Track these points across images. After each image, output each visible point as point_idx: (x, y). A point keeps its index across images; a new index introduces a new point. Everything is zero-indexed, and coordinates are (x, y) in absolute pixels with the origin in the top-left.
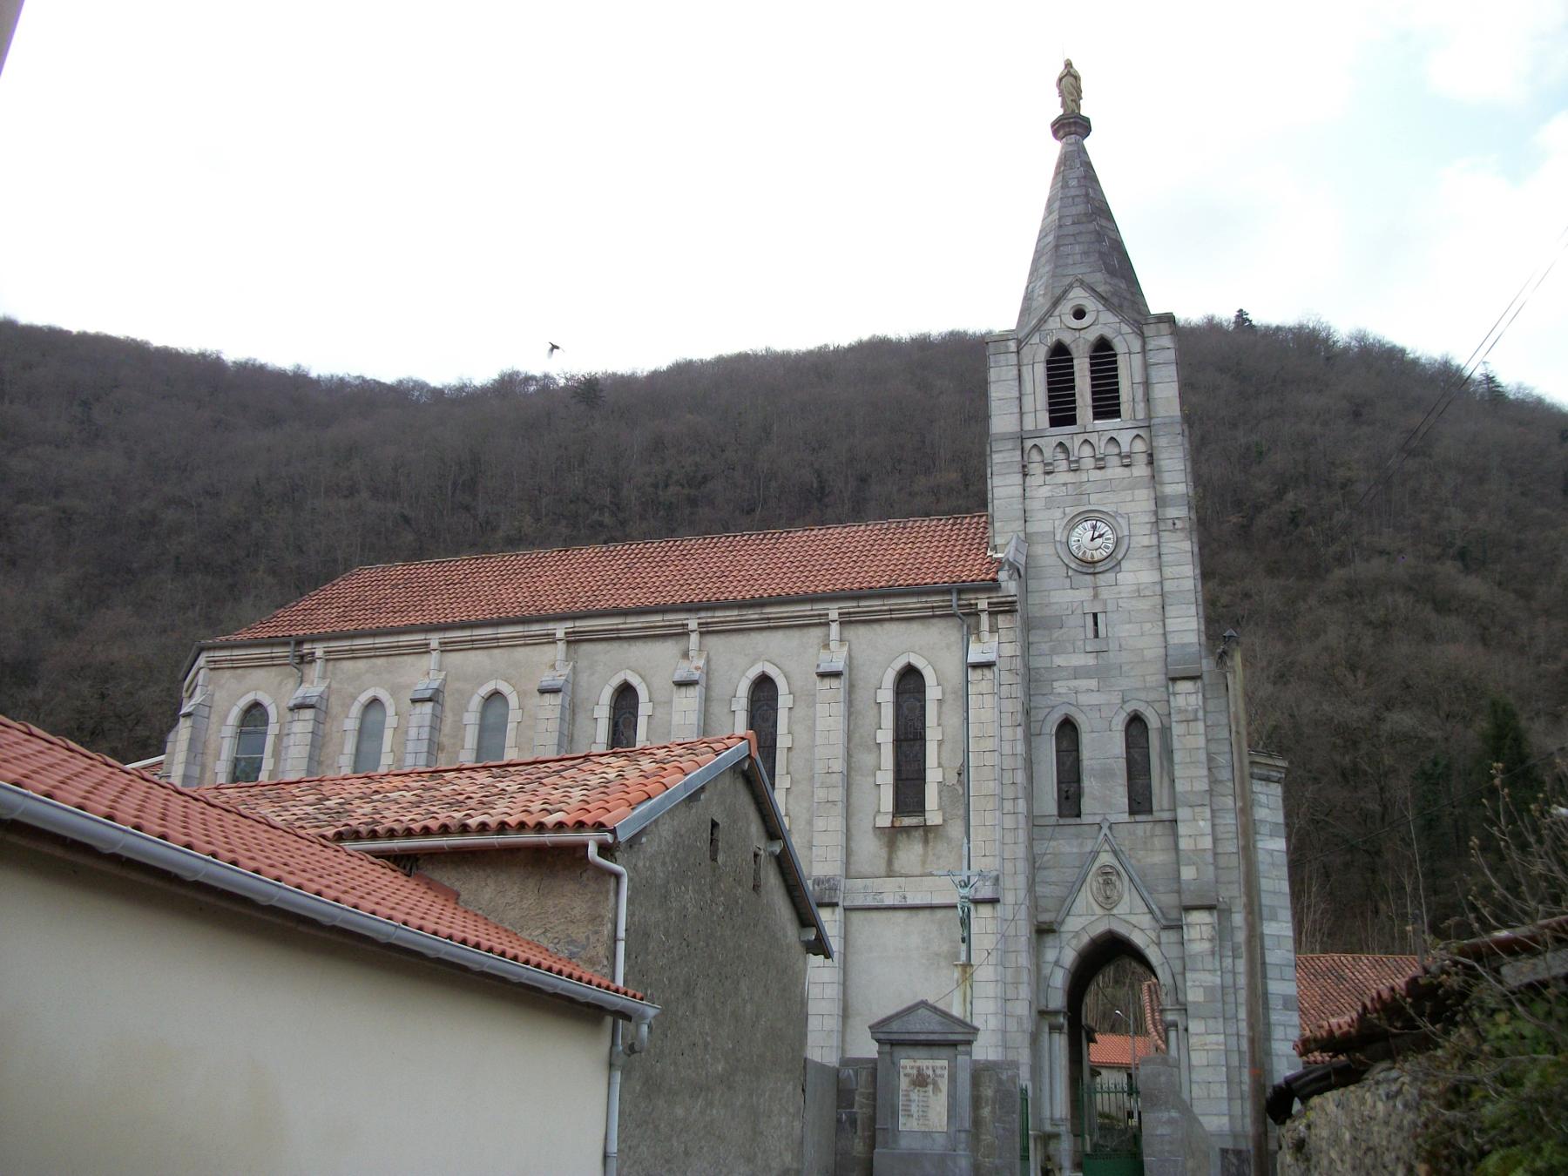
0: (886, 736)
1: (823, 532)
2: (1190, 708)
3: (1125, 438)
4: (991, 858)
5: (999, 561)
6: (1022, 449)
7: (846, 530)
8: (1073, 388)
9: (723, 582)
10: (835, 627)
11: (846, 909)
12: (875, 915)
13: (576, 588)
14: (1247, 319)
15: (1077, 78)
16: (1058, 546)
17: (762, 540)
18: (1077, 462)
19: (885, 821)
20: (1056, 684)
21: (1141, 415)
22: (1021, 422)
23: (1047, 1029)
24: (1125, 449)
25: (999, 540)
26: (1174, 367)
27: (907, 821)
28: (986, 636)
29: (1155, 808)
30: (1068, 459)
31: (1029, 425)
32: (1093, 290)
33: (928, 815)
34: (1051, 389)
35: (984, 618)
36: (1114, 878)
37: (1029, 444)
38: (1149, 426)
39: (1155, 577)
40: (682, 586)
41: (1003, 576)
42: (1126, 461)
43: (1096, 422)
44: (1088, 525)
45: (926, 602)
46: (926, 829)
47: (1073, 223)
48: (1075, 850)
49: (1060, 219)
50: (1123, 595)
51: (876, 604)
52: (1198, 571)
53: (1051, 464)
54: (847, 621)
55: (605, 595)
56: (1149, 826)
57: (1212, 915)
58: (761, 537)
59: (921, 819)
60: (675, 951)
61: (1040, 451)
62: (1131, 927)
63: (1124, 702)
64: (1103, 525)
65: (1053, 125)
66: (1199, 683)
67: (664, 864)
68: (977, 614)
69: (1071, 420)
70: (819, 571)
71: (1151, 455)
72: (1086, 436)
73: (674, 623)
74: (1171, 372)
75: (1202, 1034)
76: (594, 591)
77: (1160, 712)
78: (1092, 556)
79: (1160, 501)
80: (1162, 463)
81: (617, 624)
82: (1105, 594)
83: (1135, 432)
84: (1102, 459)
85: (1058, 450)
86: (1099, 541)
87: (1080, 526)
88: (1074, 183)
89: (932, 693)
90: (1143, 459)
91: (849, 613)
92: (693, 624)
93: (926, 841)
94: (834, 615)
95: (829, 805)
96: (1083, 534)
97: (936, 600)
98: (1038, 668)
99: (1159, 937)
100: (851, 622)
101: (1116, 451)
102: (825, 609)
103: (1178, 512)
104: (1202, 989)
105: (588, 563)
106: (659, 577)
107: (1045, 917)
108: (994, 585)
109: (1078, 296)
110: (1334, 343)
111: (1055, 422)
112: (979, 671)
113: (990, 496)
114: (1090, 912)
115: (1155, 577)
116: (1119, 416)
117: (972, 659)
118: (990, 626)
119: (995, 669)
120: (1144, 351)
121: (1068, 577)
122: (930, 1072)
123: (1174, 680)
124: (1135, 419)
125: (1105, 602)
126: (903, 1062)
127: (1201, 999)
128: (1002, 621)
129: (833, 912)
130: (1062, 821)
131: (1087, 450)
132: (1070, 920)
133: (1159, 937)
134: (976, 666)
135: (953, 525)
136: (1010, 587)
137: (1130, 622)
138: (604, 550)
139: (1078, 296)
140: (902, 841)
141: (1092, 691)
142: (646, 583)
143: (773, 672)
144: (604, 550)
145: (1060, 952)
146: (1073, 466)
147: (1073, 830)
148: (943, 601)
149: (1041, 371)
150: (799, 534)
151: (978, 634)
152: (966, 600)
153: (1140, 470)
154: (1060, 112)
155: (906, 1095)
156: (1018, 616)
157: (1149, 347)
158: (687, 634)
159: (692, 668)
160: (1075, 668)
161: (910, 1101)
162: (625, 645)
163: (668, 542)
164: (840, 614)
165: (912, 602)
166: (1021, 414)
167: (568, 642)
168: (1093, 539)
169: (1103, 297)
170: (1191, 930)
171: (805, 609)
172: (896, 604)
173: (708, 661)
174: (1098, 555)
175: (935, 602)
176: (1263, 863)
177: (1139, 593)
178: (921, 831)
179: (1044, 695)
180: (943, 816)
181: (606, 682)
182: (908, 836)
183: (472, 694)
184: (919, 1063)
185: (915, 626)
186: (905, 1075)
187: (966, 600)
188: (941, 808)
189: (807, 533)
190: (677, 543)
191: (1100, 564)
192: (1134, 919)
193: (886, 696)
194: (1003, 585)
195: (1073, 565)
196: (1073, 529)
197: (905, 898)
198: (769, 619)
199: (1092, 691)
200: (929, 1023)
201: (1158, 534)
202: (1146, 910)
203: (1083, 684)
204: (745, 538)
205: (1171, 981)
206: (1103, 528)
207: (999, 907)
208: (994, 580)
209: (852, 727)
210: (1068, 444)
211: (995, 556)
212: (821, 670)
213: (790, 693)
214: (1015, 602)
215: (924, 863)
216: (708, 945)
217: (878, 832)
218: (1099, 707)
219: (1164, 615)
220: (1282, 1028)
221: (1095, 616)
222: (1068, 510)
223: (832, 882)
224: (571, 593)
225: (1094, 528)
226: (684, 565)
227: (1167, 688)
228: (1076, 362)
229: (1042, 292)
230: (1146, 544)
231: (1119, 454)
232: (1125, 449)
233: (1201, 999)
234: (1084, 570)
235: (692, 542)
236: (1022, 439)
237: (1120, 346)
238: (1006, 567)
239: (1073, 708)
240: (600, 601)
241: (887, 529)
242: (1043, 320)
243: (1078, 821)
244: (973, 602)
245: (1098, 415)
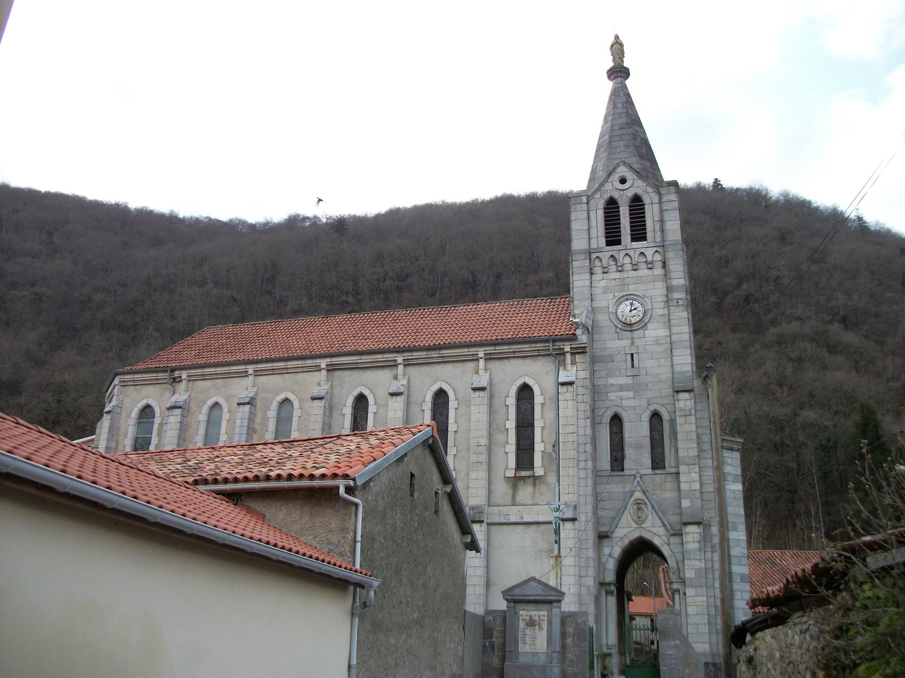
0: (511, 424)
1: (475, 307)
2: (687, 408)
3: (649, 253)
4: (572, 495)
5: (577, 323)
6: (590, 259)
7: (488, 305)
8: (619, 224)
9: (417, 336)
10: (482, 362)
11: (488, 524)
12: (505, 528)
13: (333, 339)
15: (621, 45)
16: (611, 315)
17: (440, 311)
18: (621, 266)
19: (511, 473)
20: (609, 395)
21: (658, 239)
22: (590, 243)
23: (604, 593)
24: (649, 259)
25: (576, 312)
26: (677, 212)
27: (524, 473)
28: (569, 366)
29: (666, 466)
30: (616, 265)
31: (594, 245)
32: (631, 167)
33: (535, 470)
34: (607, 224)
35: (568, 356)
36: (643, 506)
37: (594, 256)
38: (663, 246)
39: (667, 333)
40: (394, 338)
41: (579, 332)
42: (650, 266)
43: (633, 243)
44: (628, 303)
45: (535, 347)
46: (535, 478)
47: (620, 129)
48: (620, 490)
49: (612, 126)
50: (648, 343)
51: (505, 348)
52: (691, 329)
53: (606, 267)
54: (489, 358)
55: (349, 343)
56: (663, 476)
57: (699, 528)
58: (439, 309)
59: (532, 472)
60: (389, 548)
61: (601, 260)
62: (653, 534)
63: (649, 405)
64: (637, 303)
65: (608, 72)
66: (692, 394)
67: (383, 498)
68: (564, 354)
69: (618, 242)
70: (473, 329)
71: (664, 262)
72: (627, 251)
73: (389, 359)
74: (676, 215)
75: (694, 596)
76: (343, 341)
77: (670, 411)
78: (630, 320)
79: (669, 289)
80: (671, 267)
81: (356, 360)
82: (638, 342)
83: (655, 249)
84: (636, 265)
85: (611, 259)
86: (634, 312)
87: (623, 304)
88: (620, 105)
89: (538, 399)
90: (660, 264)
91: (490, 354)
92: (400, 360)
93: (534, 485)
94: (481, 354)
95: (479, 464)
96: (625, 308)
97: (540, 346)
98: (599, 385)
99: (669, 540)
100: (491, 359)
101: (644, 260)
102: (476, 351)
103: (680, 295)
104: (694, 570)
105: (339, 324)
106: (380, 333)
107: (603, 529)
108: (574, 337)
109: (622, 171)
110: (770, 197)
111: (609, 243)
112: (565, 387)
113: (571, 286)
114: (629, 526)
115: (667, 333)
116: (646, 240)
117: (561, 380)
119: (575, 385)
120: (660, 202)
121: (616, 332)
122: (537, 618)
123: (678, 392)
124: (655, 242)
126: (521, 612)
127: (693, 576)
128: (578, 358)
129: (481, 526)
130: (613, 474)
131: (627, 260)
133: (669, 540)
134: (563, 384)
135: (550, 303)
136: (583, 338)
137: (652, 359)
138: (348, 317)
139: (622, 171)
140: (521, 485)
141: (631, 398)
142: (373, 336)
143: (446, 387)
144: (348, 317)
145: (612, 549)
146: (620, 269)
147: (619, 478)
148: (544, 347)
149: (601, 214)
150: (461, 308)
151: (564, 366)
152: (557, 346)
153: (658, 271)
154: (612, 64)
155: (523, 632)
156: (587, 355)
157: (663, 200)
158: (396, 366)
159: (399, 385)
160: (621, 385)
161: (525, 635)
162: (361, 372)
163: (386, 312)
164: (485, 354)
165: (526, 347)
166: (590, 238)
167: (328, 370)
168: (631, 311)
169: (636, 171)
170: (687, 536)
171: (465, 351)
172: (517, 348)
173: (409, 381)
175: (540, 347)
176: (729, 497)
177: (657, 342)
178: (532, 479)
179: (602, 401)
180: (544, 470)
181: (350, 393)
182: (524, 482)
183: (273, 400)
184: (530, 613)
185: (528, 361)
186: (522, 620)
187: (557, 346)
188: (543, 466)
189: (466, 307)
190: (391, 313)
191: (635, 325)
192: (654, 530)
193: (512, 401)
194: (579, 337)
195: (619, 326)
196: (619, 305)
197: (522, 518)
198: (444, 357)
199: (631, 398)
200: (536, 590)
201: (668, 308)
202: (661, 525)
203: (625, 394)
204: (430, 310)
205: (676, 566)
206: (636, 305)
207: (576, 523)
208: (574, 334)
209: (491, 419)
210: (616, 256)
211: (574, 320)
212: (474, 386)
213: (456, 400)
214: (586, 347)
215: (533, 497)
216: (408, 545)
217: (507, 480)
218: (634, 408)
219: (672, 354)
220: (740, 593)
221: (632, 355)
222: (616, 294)
224: (330, 342)
225: (632, 304)
226: (395, 326)
227: (674, 397)
228: (621, 209)
230: (662, 313)
231: (646, 262)
232: (649, 259)
233: (693, 576)
234: (626, 329)
235: (400, 313)
236: (590, 253)
237: (646, 200)
238: (581, 327)
239: (619, 408)
240: (346, 346)
241: (512, 305)
242: (602, 185)
243: (622, 473)
244: (561, 347)
245: (634, 239)
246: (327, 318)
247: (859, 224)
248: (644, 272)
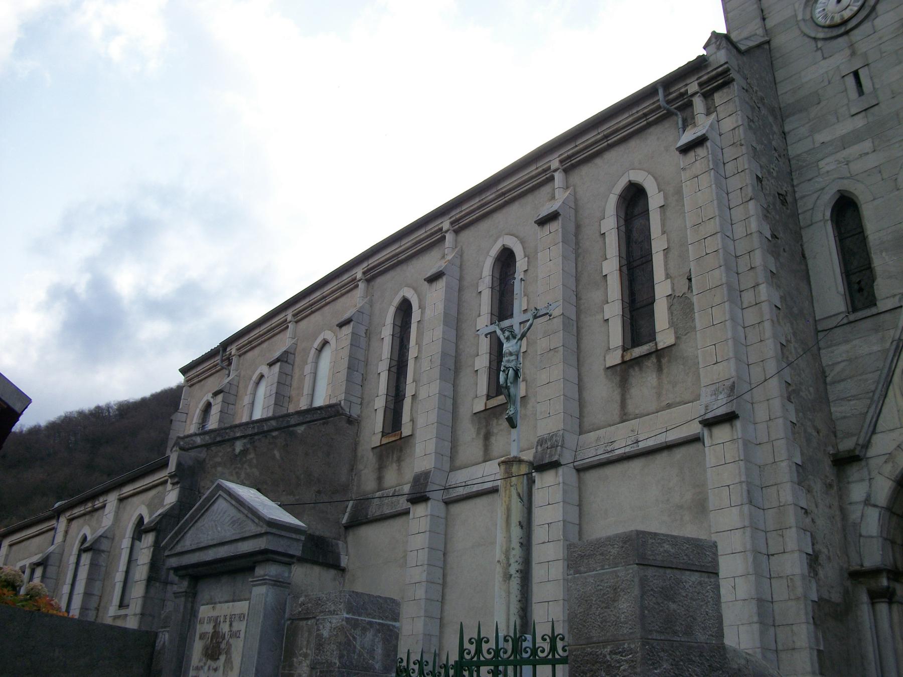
0: (611, 266)
4: (725, 363)
11: (579, 470)
12: (609, 471)
16: (802, 24)
19: (615, 358)
23: (865, 598)
27: (638, 352)
33: (659, 338)
46: (659, 354)
48: (875, 348)
59: (652, 344)
82: (862, 47)
93: (660, 369)
95: (552, 352)
98: (799, 155)
107: (846, 445)
121: (818, 49)
125: (865, 55)
129: (557, 473)
132: (876, 439)
141: (867, 154)
145: (870, 487)
147: (868, 324)
152: (675, 92)
156: (735, 87)
160: (842, 138)
162: (404, 267)
174: (847, 14)
178: (653, 359)
179: (809, 180)
180: (676, 333)
181: (390, 304)
182: (641, 369)
183: (311, 348)
185: (633, 143)
187: (675, 92)
188: (672, 324)
199: (867, 154)
203: (854, 150)
207: (738, 424)
209: (579, 269)
215: (659, 395)
217: (609, 372)
218: (879, 169)
223: (554, 438)
239: (845, 181)
243: (874, 310)
244: (683, 90)
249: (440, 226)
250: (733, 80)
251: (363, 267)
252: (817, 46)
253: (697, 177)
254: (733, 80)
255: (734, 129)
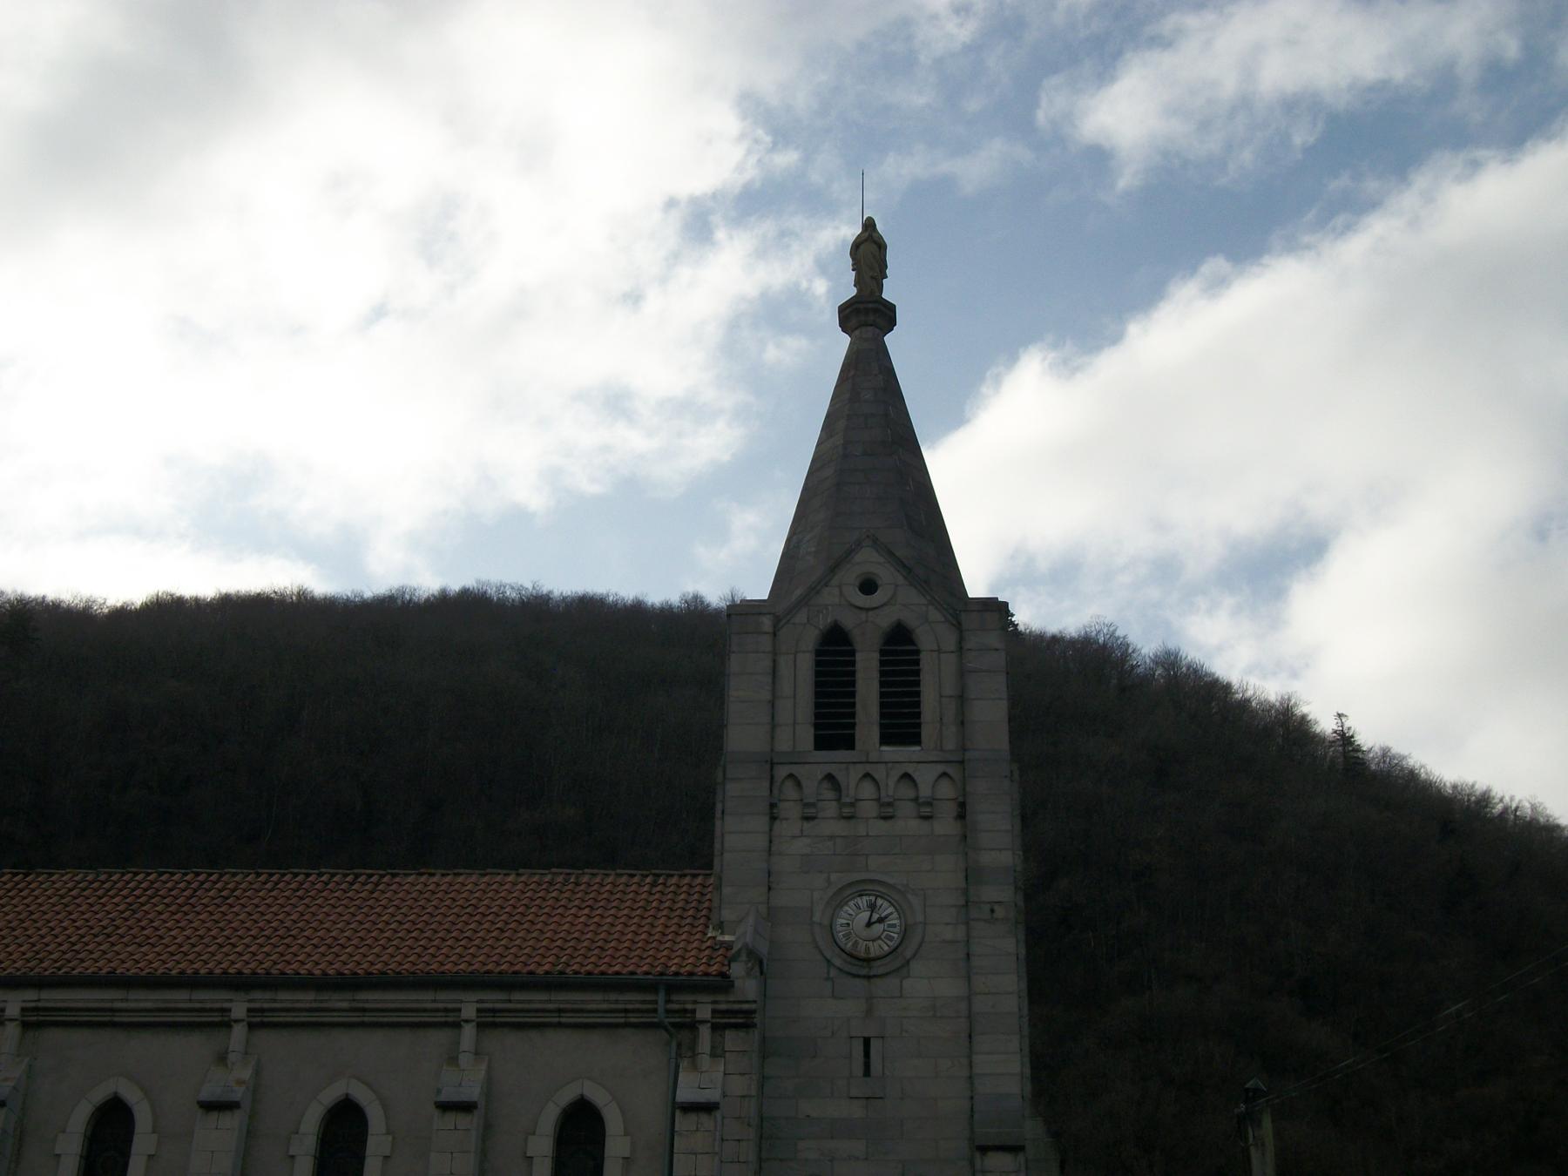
1: (448, 879)
3: (926, 777)
5: (728, 946)
6: (772, 778)
7: (486, 879)
8: (853, 694)
9: (288, 946)
10: (469, 1031)
13: (43, 937)
14: (1012, 623)
15: (881, 246)
17: (352, 884)
18: (852, 805)
21: (950, 744)
22: (773, 738)
24: (925, 791)
25: (727, 915)
26: (1002, 678)
28: (705, 1061)
30: (838, 800)
31: (784, 744)
32: (891, 553)
35: (705, 1033)
37: (782, 771)
38: (962, 762)
40: (221, 946)
41: (737, 970)
42: (926, 810)
43: (884, 748)
44: (863, 902)
45: (617, 1002)
51: (537, 999)
52: (1024, 985)
53: (813, 805)
54: (488, 1022)
55: (91, 952)
58: (349, 878)
61: (799, 784)
64: (886, 904)
65: (839, 307)
66: (1021, 1157)
68: (693, 1026)
69: (849, 743)
70: (443, 940)
71: (963, 805)
72: (868, 768)
73: (208, 1006)
74: (999, 683)
76: (73, 944)
78: (868, 949)
79: (972, 875)
81: (112, 1001)
83: (940, 768)
84: (890, 804)
85: (826, 785)
86: (878, 928)
87: (851, 903)
89: (616, 1146)
90: (949, 810)
91: (494, 1011)
92: (239, 1010)
94: (469, 1011)
96: (854, 915)
97: (633, 999)
100: (495, 1025)
101: (911, 794)
102: (227, 1001)
103: (1001, 894)
105: (62, 897)
106: (183, 929)
108: (724, 983)
109: (868, 561)
110: (1133, 667)
111: (822, 743)
112: (693, 1117)
113: (717, 846)
117: (685, 1094)
118: (713, 1048)
119: (718, 1114)
120: (960, 649)
121: (828, 979)
123: (984, 1149)
124: (942, 750)
128: (731, 1039)
131: (868, 790)
135: (654, 884)
136: (747, 987)
138: (89, 878)
139: (868, 561)
142: (161, 938)
143: (362, 1095)
144: (89, 878)
146: (846, 811)
148: (644, 1002)
149: (806, 663)
150: (410, 879)
151: (694, 1056)
152: (678, 1002)
153: (946, 826)
154: (853, 292)
158: (227, 1025)
159: (229, 1081)
163: (198, 874)
164: (479, 1010)
165: (594, 1000)
166: (773, 727)
167: (26, 1026)
168: (869, 924)
169: (904, 566)
171: (425, 998)
172: (568, 1002)
173: (257, 1073)
175: (630, 1002)
179: (781, 1160)
187: (678, 1002)
189: (423, 879)
190: (213, 878)
191: (878, 963)
193: (542, 1146)
194: (737, 983)
195: (837, 962)
196: (841, 905)
198: (364, 1010)
201: (967, 924)
204: (324, 878)
206: (886, 909)
208: (723, 975)
210: (840, 777)
211: (720, 938)
212: (443, 1098)
213: (388, 1133)
214: (753, 1012)
219: (970, 1048)
221: (867, 1042)
222: (834, 877)
224: (33, 945)
225: (872, 907)
226: (224, 914)
227: (972, 1163)
228: (859, 657)
229: (813, 549)
231: (916, 799)
232: (925, 791)
234: (854, 970)
235: (238, 878)
236: (772, 764)
238: (744, 957)
240: (82, 961)
241: (551, 883)
242: (814, 590)
244: (689, 1006)
245: (886, 739)
246: (26, 875)
247: (1345, 754)
248: (908, 824)
249: (226, 1005)
250: (754, 1026)
251: (25, 998)
252: (828, 973)
253: (695, 1154)
254: (754, 1026)
255: (743, 1097)
